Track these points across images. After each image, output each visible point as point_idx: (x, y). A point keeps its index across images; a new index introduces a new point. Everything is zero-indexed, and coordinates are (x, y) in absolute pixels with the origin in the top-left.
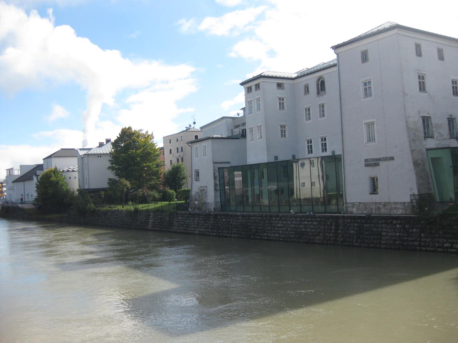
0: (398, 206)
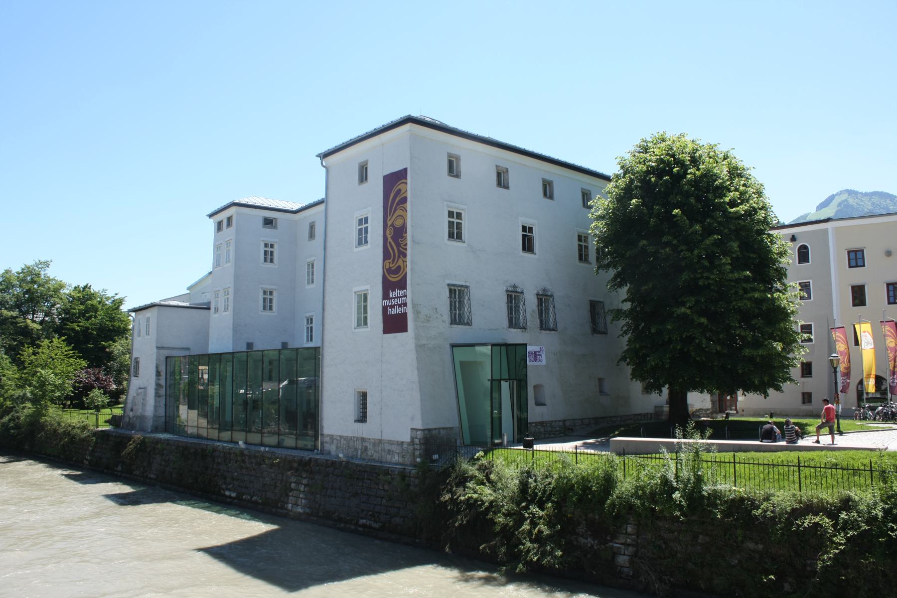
0: (394, 448)
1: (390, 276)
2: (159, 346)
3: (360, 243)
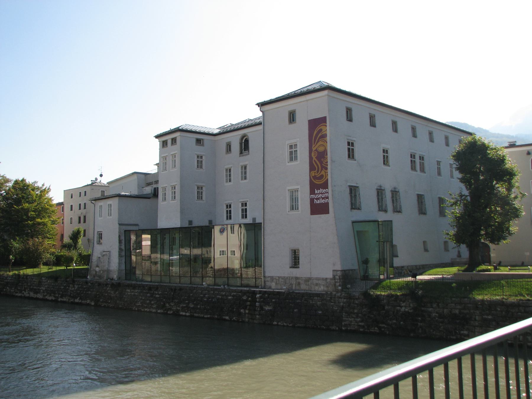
0: (320, 282)
1: (315, 181)
2: (120, 223)
3: (291, 159)
